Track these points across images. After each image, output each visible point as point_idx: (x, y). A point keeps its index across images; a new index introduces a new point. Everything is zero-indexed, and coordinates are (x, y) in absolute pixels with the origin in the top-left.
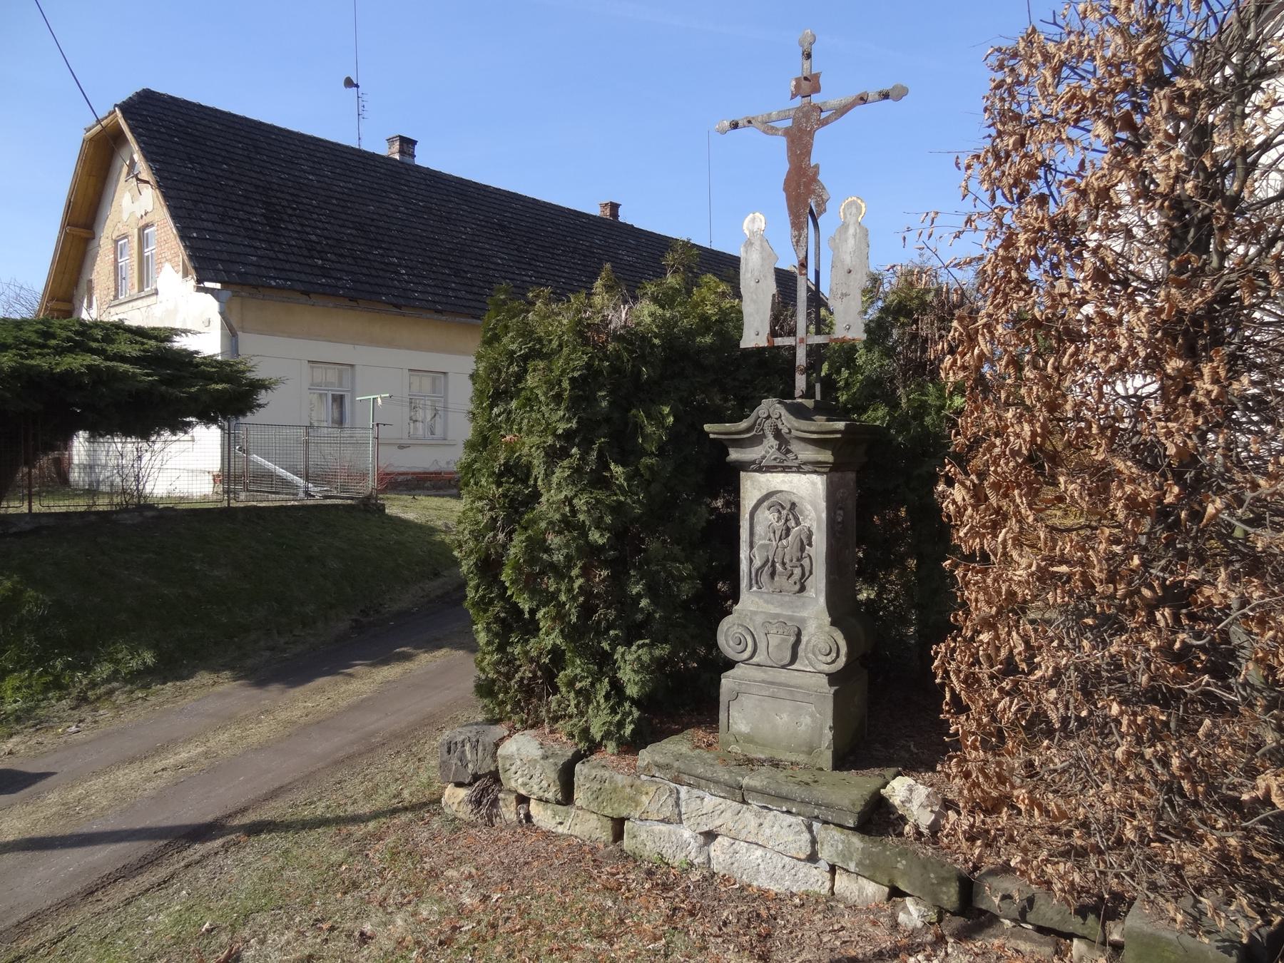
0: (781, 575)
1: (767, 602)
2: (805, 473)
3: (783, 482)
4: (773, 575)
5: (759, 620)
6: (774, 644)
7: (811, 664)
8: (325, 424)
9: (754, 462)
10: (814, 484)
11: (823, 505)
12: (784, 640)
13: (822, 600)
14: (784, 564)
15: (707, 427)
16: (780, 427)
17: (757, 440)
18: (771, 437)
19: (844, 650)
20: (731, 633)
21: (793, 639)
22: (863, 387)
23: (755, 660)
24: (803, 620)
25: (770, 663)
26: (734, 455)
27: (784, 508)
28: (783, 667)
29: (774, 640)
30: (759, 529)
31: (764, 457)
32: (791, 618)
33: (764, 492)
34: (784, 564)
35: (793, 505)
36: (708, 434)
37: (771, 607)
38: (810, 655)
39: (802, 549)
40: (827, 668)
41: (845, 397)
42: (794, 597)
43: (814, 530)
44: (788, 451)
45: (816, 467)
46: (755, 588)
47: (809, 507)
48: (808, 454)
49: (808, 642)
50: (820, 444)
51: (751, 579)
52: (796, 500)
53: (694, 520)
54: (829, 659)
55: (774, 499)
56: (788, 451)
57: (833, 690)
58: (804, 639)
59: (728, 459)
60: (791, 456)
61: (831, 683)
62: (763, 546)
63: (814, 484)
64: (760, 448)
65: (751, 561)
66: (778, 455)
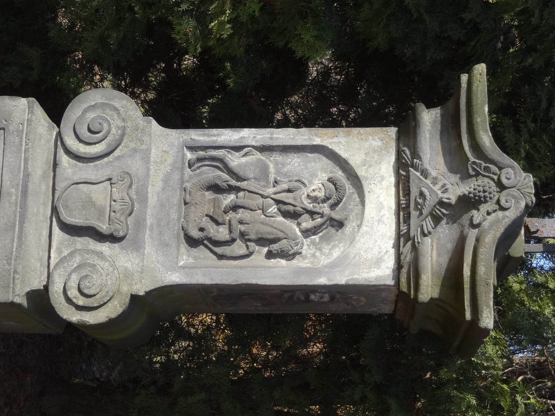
0: (216, 203)
1: (167, 180)
2: (397, 246)
3: (381, 206)
4: (215, 188)
5: (135, 165)
6: (93, 195)
7: (62, 261)
8: (188, 196)
9: (415, 154)
10: (378, 262)
11: (341, 279)
12: (101, 211)
13: (175, 278)
14: (235, 208)
15: (481, 69)
16: (484, 208)
17: (458, 164)
18: (464, 189)
19: (91, 318)
20: (109, 114)
21: (104, 227)
22: (534, 315)
23: (64, 159)
24: (137, 246)
25: (60, 186)
26: (429, 118)
27: (333, 207)
28: (55, 210)
29: (99, 194)
30: (294, 163)
31: (425, 173)
32: (140, 224)
33: (361, 172)
34: (235, 208)
35: (340, 225)
36: (469, 71)
37: (159, 185)
38: (77, 259)
39: (262, 241)
40: (56, 289)
41: (516, 287)
42: (177, 228)
43: (296, 262)
44: (437, 220)
45: (408, 266)
46: (189, 155)
47: (336, 253)
48: (434, 255)
49: (100, 255)
50: (452, 277)
51: (205, 148)
52: (348, 229)
53: (307, 37)
54: (73, 293)
55: (349, 189)
56: (437, 220)
57: (21, 300)
58: (105, 248)
59: (421, 108)
60: (428, 224)
61: (32, 295)
63: (378, 262)
64: (443, 167)
65: (237, 149)
66: (431, 201)
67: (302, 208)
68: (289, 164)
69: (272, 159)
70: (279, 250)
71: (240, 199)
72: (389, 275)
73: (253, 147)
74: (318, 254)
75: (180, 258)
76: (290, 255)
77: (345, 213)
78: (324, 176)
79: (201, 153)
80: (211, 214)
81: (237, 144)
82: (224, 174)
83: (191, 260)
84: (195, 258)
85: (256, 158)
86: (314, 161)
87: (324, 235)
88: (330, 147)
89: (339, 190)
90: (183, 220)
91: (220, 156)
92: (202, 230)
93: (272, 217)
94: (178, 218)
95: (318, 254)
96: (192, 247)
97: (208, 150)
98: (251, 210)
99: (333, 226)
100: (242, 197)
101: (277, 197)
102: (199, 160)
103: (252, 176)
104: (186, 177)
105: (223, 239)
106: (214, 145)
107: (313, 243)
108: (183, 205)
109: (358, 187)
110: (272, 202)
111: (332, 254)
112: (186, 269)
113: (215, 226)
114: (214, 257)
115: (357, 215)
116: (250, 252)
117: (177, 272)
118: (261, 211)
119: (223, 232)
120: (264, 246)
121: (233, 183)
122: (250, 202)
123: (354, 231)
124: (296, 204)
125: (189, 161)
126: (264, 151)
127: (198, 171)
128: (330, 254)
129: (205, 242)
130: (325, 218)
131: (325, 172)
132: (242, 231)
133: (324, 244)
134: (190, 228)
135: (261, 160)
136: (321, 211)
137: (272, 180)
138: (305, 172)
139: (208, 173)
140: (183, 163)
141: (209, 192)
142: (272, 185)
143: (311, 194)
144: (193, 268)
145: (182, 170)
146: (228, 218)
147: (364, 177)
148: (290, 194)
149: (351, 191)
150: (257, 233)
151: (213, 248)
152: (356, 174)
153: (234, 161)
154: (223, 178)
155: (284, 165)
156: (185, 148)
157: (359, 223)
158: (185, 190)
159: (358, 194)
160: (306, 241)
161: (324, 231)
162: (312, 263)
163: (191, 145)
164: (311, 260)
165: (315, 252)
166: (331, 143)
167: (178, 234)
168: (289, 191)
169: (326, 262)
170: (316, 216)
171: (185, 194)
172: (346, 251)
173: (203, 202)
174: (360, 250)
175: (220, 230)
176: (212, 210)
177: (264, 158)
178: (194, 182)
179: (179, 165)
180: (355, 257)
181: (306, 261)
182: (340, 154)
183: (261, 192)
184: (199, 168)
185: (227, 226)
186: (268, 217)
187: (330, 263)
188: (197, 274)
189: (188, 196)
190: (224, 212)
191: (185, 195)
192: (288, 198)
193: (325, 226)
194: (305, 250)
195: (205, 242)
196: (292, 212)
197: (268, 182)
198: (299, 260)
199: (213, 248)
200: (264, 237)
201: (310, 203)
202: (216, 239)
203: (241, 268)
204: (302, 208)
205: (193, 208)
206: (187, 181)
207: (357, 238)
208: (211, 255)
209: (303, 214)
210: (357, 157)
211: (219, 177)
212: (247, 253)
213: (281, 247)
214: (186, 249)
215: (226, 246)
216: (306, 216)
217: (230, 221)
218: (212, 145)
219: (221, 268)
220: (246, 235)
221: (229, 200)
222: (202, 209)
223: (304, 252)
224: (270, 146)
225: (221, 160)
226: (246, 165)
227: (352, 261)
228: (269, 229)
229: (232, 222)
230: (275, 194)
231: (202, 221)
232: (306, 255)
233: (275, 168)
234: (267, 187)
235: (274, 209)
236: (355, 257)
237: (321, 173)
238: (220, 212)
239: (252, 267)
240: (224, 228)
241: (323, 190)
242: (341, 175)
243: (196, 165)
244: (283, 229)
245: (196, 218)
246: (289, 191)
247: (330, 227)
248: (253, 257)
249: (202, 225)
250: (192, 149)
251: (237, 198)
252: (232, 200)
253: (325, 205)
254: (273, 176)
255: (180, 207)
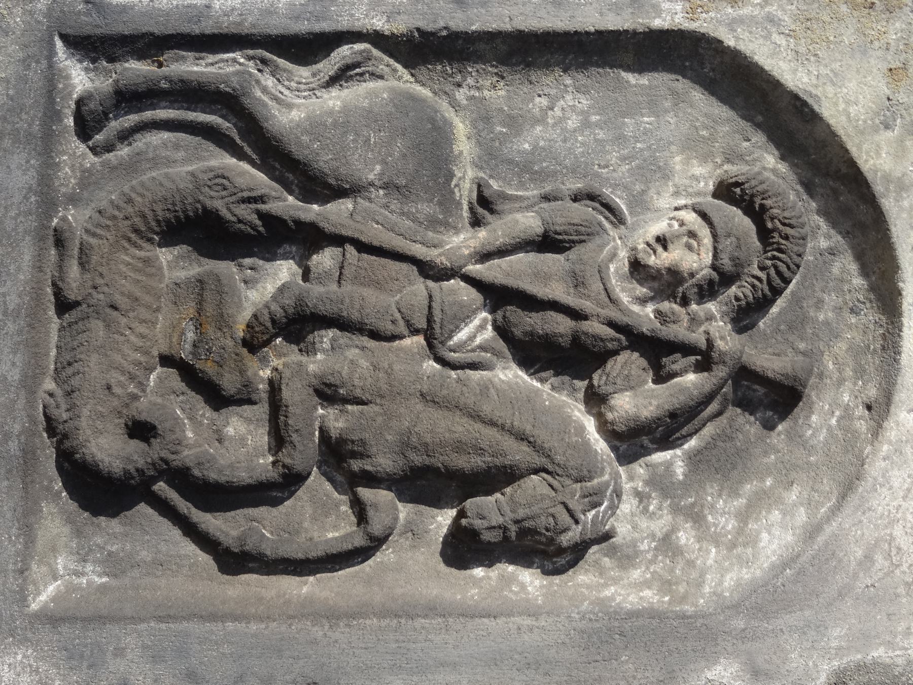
4: (203, 230)
8: (74, 270)
14: (298, 324)
27: (745, 317)
30: (563, 113)
33: (875, 157)
34: (298, 324)
35: (777, 398)
39: (425, 483)
46: (80, 78)
47: (775, 538)
51: (152, 45)
52: (820, 418)
55: (821, 237)
62: (431, 149)
67: (611, 324)
68: (541, 120)
69: (461, 95)
70: (513, 528)
71: (320, 280)
72: (493, 338)
73: (377, 39)
74: (685, 537)
75: (37, 570)
76: (561, 551)
77: (802, 346)
78: (702, 176)
79: (137, 69)
80: (185, 353)
81: (303, 27)
82: (245, 166)
83: (94, 577)
84: (114, 565)
85: (392, 90)
86: (653, 107)
87: (709, 447)
88: (730, 42)
89: (777, 238)
90: (49, 384)
91: (226, 80)
92: (141, 430)
93: (474, 366)
94: (25, 377)
95: (685, 537)
96: (96, 513)
97: (168, 55)
98: (375, 335)
99: (746, 405)
100: (328, 274)
101: (494, 271)
102: (128, 98)
103: (373, 174)
104: (67, 177)
105: (243, 476)
106: (196, 29)
107: (660, 483)
108: (52, 312)
109: (862, 227)
110: (468, 294)
111: (753, 541)
112: (65, 629)
113: (205, 413)
114: (204, 559)
115: (857, 352)
116: (372, 538)
117: (24, 641)
118: (420, 339)
119: (242, 440)
120: (437, 502)
121: (287, 205)
122: (370, 295)
123: (855, 433)
124: (586, 305)
125: (80, 102)
126: (425, 62)
127: (124, 151)
128: (741, 540)
129: (161, 487)
130: (720, 372)
131: (705, 158)
132: (334, 434)
133: (712, 489)
134: (84, 423)
135: (413, 98)
136: (698, 338)
137: (465, 192)
138: (613, 158)
139: (171, 162)
140: (52, 115)
141: (177, 250)
142: (466, 214)
143: (652, 261)
144: (101, 619)
145: (47, 144)
146: (266, 373)
147: (887, 179)
148: (550, 258)
149: (824, 244)
150: (405, 445)
151: (198, 516)
152: (852, 164)
153: (290, 106)
154: (240, 182)
155: (516, 123)
156: (59, 44)
157: (872, 392)
158: (60, 242)
159: (859, 257)
160: (631, 478)
161: (709, 430)
162: (666, 585)
163: (88, 30)
164: (657, 567)
165: (674, 530)
166: (733, 24)
167: (28, 455)
168: (548, 243)
169: (729, 581)
170: (676, 362)
171: (62, 257)
172: (828, 530)
173: (147, 299)
174: (893, 522)
175: (230, 431)
176: (190, 335)
177: (426, 92)
178: (104, 204)
179: (30, 121)
180: (868, 558)
181: (636, 574)
182: (776, 73)
183: (418, 250)
184: (125, 136)
185: (262, 410)
186: (454, 366)
187: (755, 588)
188: (119, 652)
189: (74, 270)
190: (245, 343)
191: (61, 266)
192: (546, 278)
193: (713, 407)
194: (629, 520)
195: (161, 487)
196: (565, 342)
197: (448, 201)
198: (602, 571)
199: (198, 516)
200: (437, 461)
201: (643, 301)
202: (213, 476)
203: (332, 615)
204: (611, 324)
205: (97, 327)
206: (73, 200)
207: (875, 468)
208: (189, 548)
209: (616, 353)
210: (852, 85)
211: (221, 177)
212: (359, 541)
213: (521, 513)
214: (69, 521)
215: (256, 504)
216: (629, 362)
217: (274, 388)
218: (185, 28)
219: (236, 618)
220: (355, 455)
221: (270, 288)
222: (142, 329)
223: (623, 530)
224: (455, 37)
225: (229, 101)
226: (345, 122)
227: (855, 576)
228: (461, 427)
229: (286, 394)
230: (485, 256)
231: (142, 386)
232: (634, 544)
233: (477, 137)
234: (447, 225)
235: (482, 327)
236: (868, 558)
237: (687, 162)
238: (227, 344)
239: (383, 613)
240: (248, 421)
241: (707, 241)
242: (774, 171)
243: (115, 125)
244: (528, 428)
245: (115, 377)
246: (548, 243)
247: (733, 411)
248: (385, 556)
249: (145, 408)
250: (92, 47)
251: (306, 276)
252: (282, 290)
253: (712, 307)
254: (470, 173)
255: (34, 321)
